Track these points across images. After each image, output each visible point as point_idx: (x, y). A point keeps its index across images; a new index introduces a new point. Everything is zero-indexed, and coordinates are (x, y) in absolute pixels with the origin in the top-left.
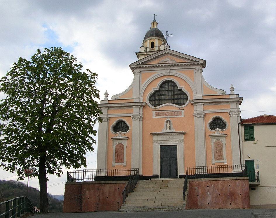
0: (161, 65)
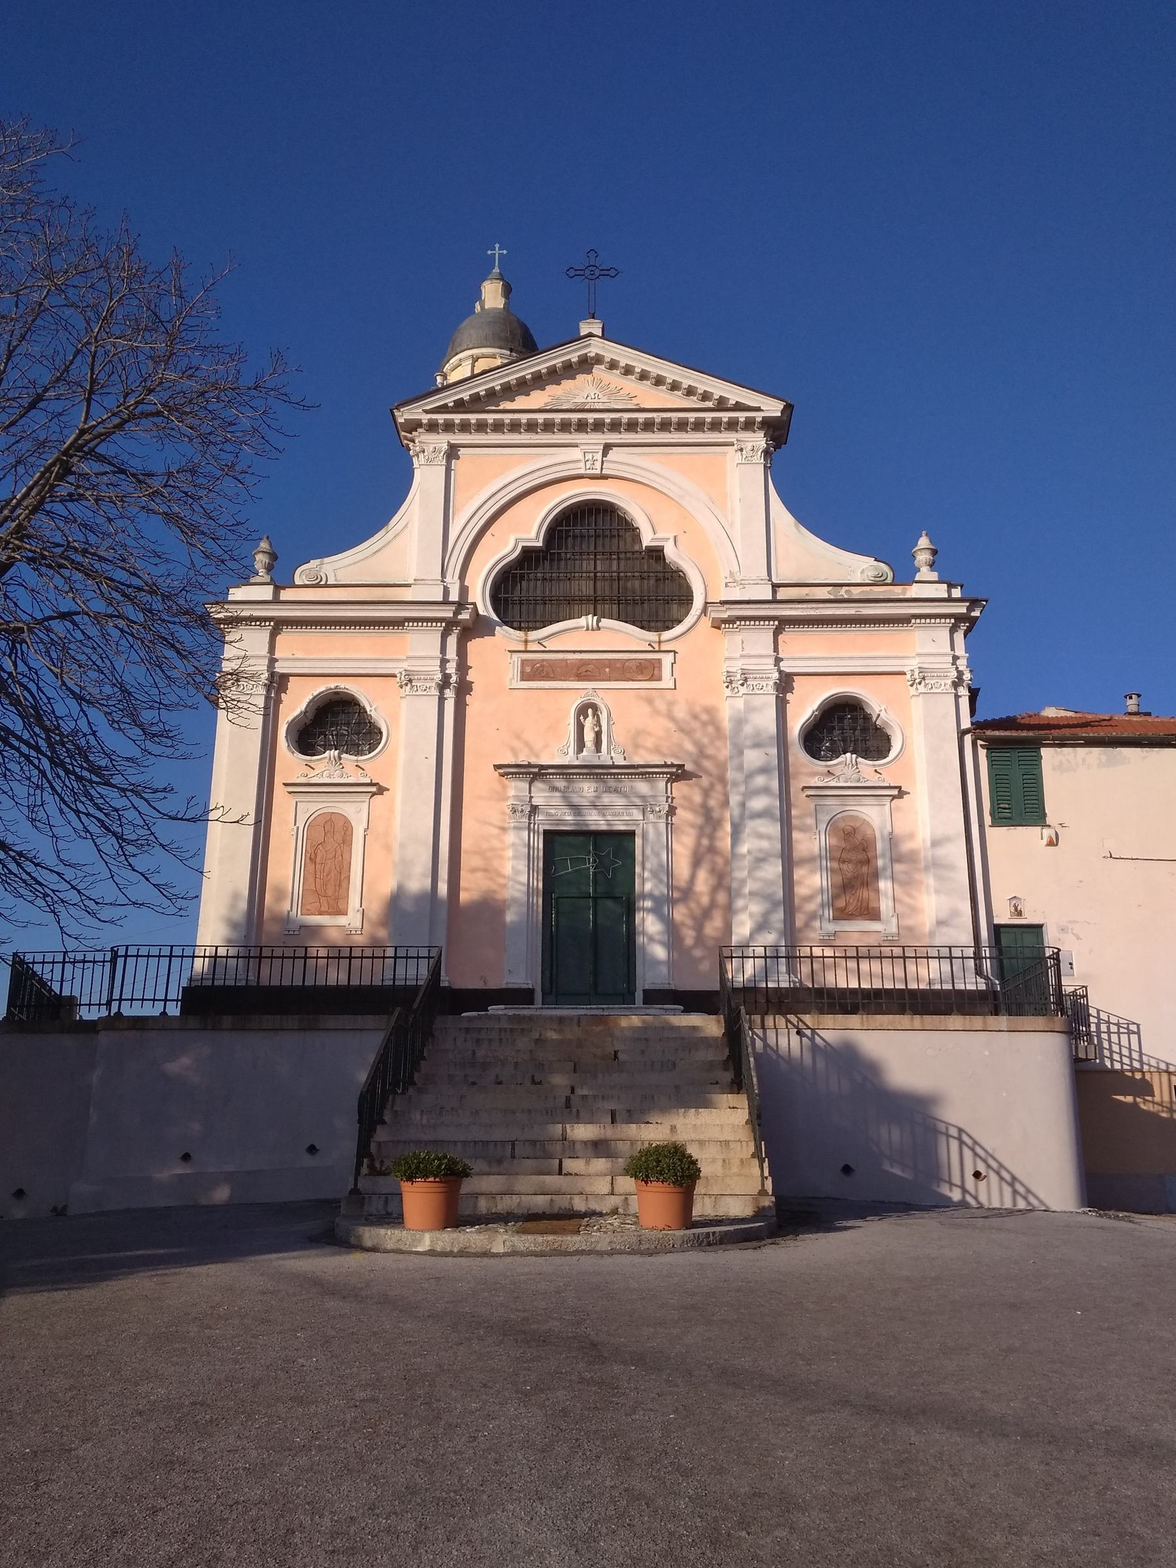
0: (580, 420)
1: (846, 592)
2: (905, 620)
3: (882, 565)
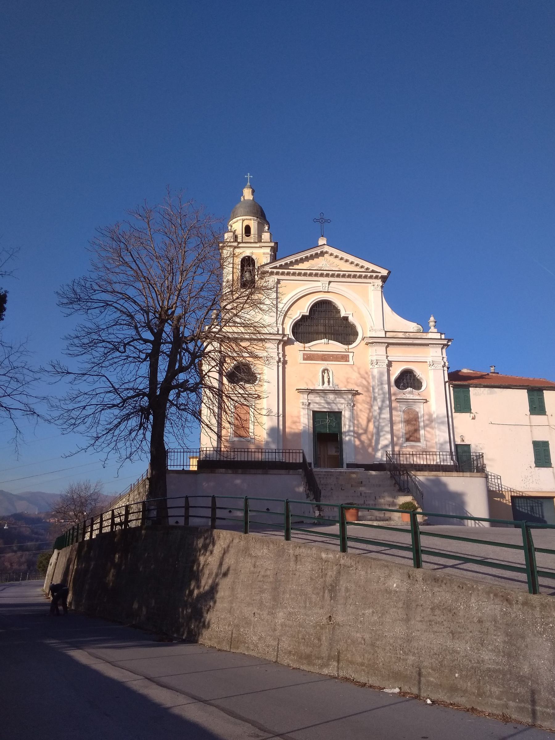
0: (321, 273)
1: (408, 334)
2: (427, 345)
3: (419, 326)
